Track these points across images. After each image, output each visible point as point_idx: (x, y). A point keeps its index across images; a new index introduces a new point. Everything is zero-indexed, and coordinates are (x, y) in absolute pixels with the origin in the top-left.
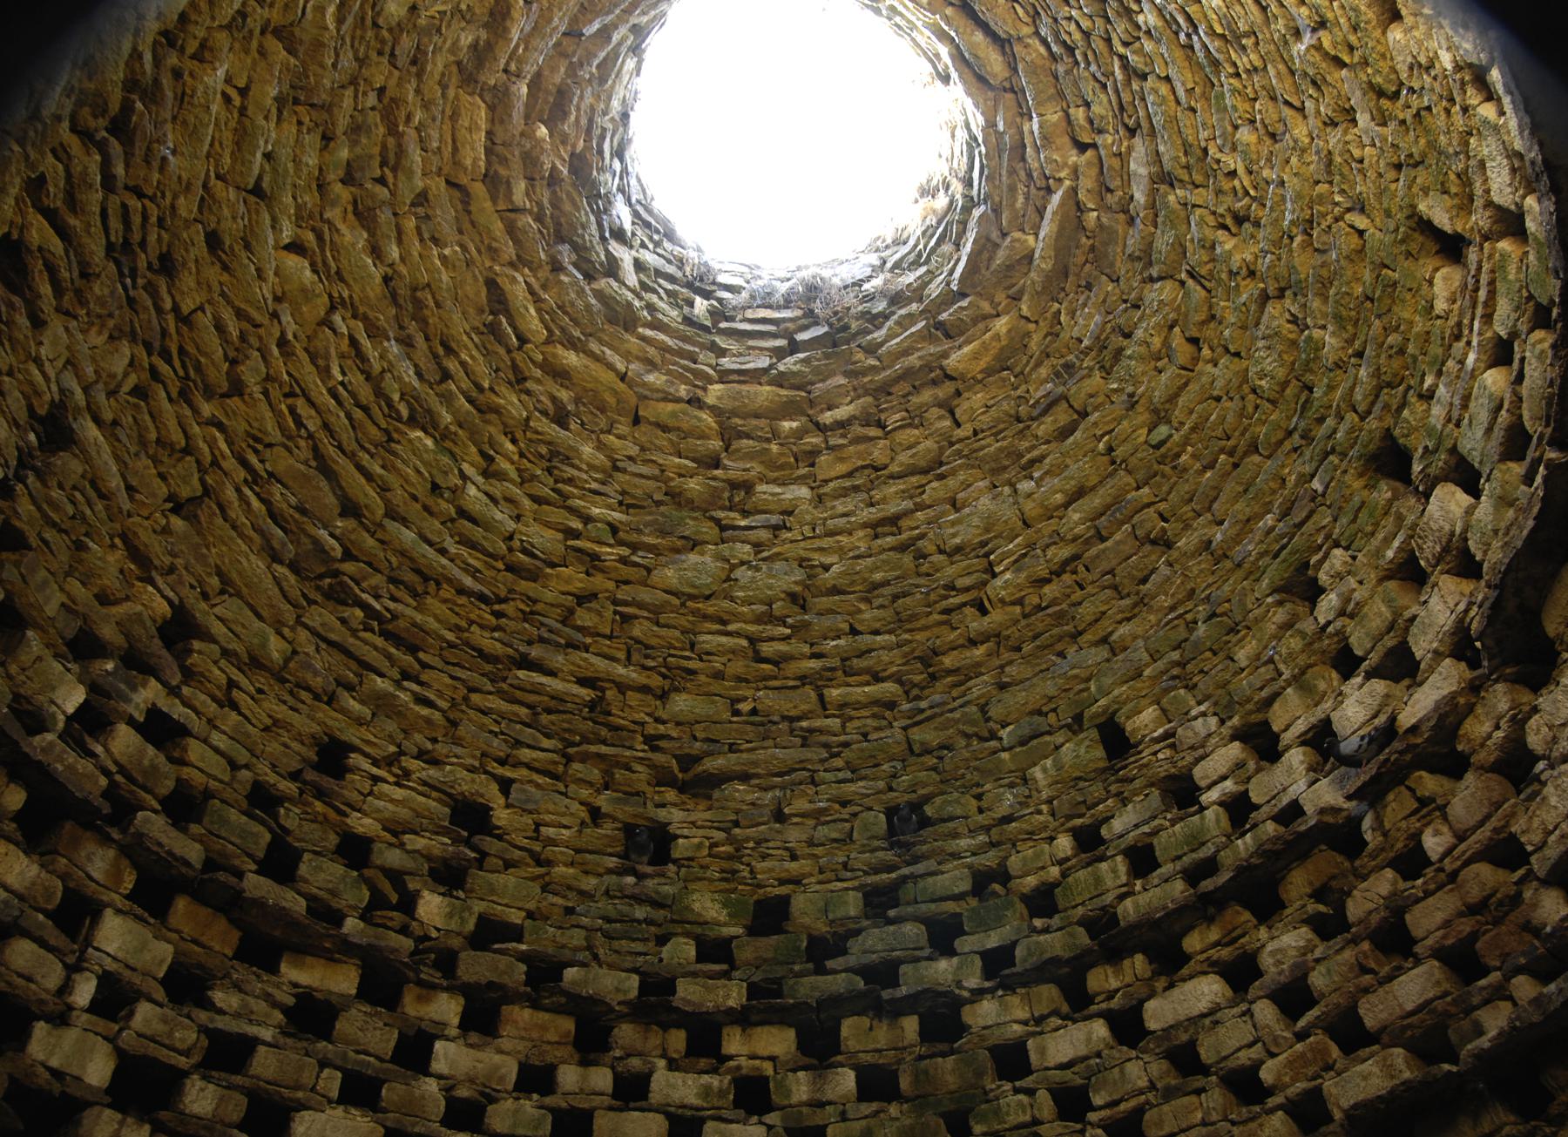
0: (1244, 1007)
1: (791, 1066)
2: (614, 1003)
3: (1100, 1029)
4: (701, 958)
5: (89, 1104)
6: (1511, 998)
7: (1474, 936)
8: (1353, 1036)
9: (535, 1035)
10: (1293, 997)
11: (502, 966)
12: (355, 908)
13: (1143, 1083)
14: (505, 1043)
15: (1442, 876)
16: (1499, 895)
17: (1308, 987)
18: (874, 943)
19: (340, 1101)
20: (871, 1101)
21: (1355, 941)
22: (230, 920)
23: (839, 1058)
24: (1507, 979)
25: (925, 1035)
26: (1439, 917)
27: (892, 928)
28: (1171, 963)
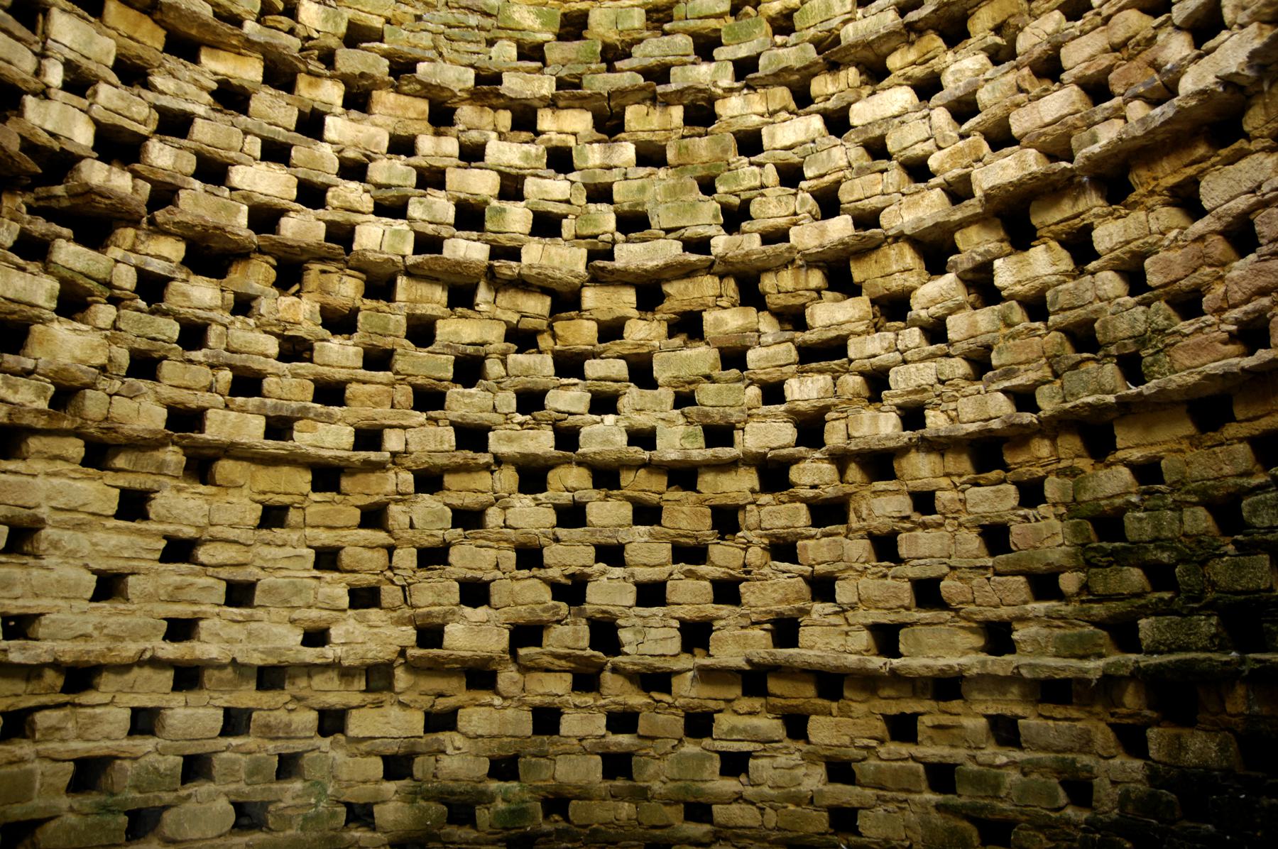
0: (925, 112)
1: (588, 139)
2: (456, 90)
3: (817, 123)
4: (521, 57)
5: (81, 158)
6: (1125, 118)
7: (1110, 69)
8: (1001, 138)
9: (399, 113)
10: (963, 109)
11: (370, 61)
12: (251, 13)
13: (843, 163)
14: (377, 118)
15: (1099, 19)
16: (1138, 37)
17: (975, 100)
18: (651, 50)
19: (263, 159)
20: (645, 166)
21: (1017, 68)
22: (156, 22)
23: (623, 135)
24: (1126, 103)
25: (688, 121)
26: (1087, 52)
27: (666, 38)
28: (876, 73)
